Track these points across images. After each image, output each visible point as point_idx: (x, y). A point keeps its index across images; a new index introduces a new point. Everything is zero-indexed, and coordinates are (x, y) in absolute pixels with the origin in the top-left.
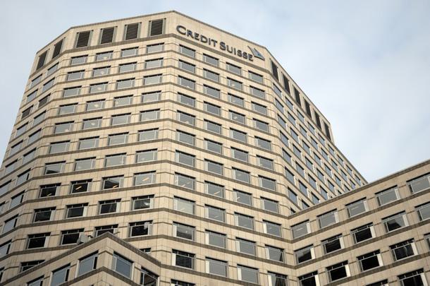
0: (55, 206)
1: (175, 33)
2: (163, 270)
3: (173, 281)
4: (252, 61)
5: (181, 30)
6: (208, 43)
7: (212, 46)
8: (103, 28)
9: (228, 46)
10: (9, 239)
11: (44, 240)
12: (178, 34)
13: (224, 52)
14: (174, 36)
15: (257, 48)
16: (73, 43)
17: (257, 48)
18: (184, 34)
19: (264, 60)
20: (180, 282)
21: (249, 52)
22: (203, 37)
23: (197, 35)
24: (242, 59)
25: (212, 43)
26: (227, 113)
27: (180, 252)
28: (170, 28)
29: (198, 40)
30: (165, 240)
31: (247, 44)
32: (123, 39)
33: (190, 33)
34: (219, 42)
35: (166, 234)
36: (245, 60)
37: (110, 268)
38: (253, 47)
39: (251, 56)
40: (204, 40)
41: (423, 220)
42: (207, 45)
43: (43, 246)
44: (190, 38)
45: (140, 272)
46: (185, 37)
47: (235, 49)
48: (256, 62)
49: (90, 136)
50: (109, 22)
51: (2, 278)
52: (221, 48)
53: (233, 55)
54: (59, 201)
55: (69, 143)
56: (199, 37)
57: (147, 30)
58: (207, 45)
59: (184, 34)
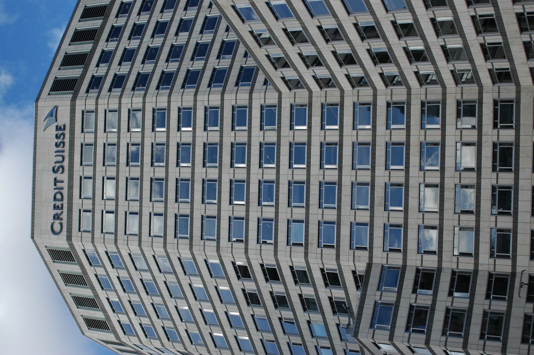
4: (64, 126)
5: (57, 228)
6: (62, 191)
7: (65, 185)
15: (365, 349)
17: (365, 349)
18: (61, 224)
19: (56, 107)
22: (55, 199)
24: (67, 140)
27: (451, 286)
29: (62, 205)
31: (40, 132)
32: (88, 288)
33: (57, 217)
37: (172, 13)
39: (58, 128)
40: (59, 196)
42: (65, 192)
48: (64, 119)
51: (396, 342)
53: (66, 154)
55: (167, 282)
56: (59, 203)
58: (65, 192)
59: (61, 224)
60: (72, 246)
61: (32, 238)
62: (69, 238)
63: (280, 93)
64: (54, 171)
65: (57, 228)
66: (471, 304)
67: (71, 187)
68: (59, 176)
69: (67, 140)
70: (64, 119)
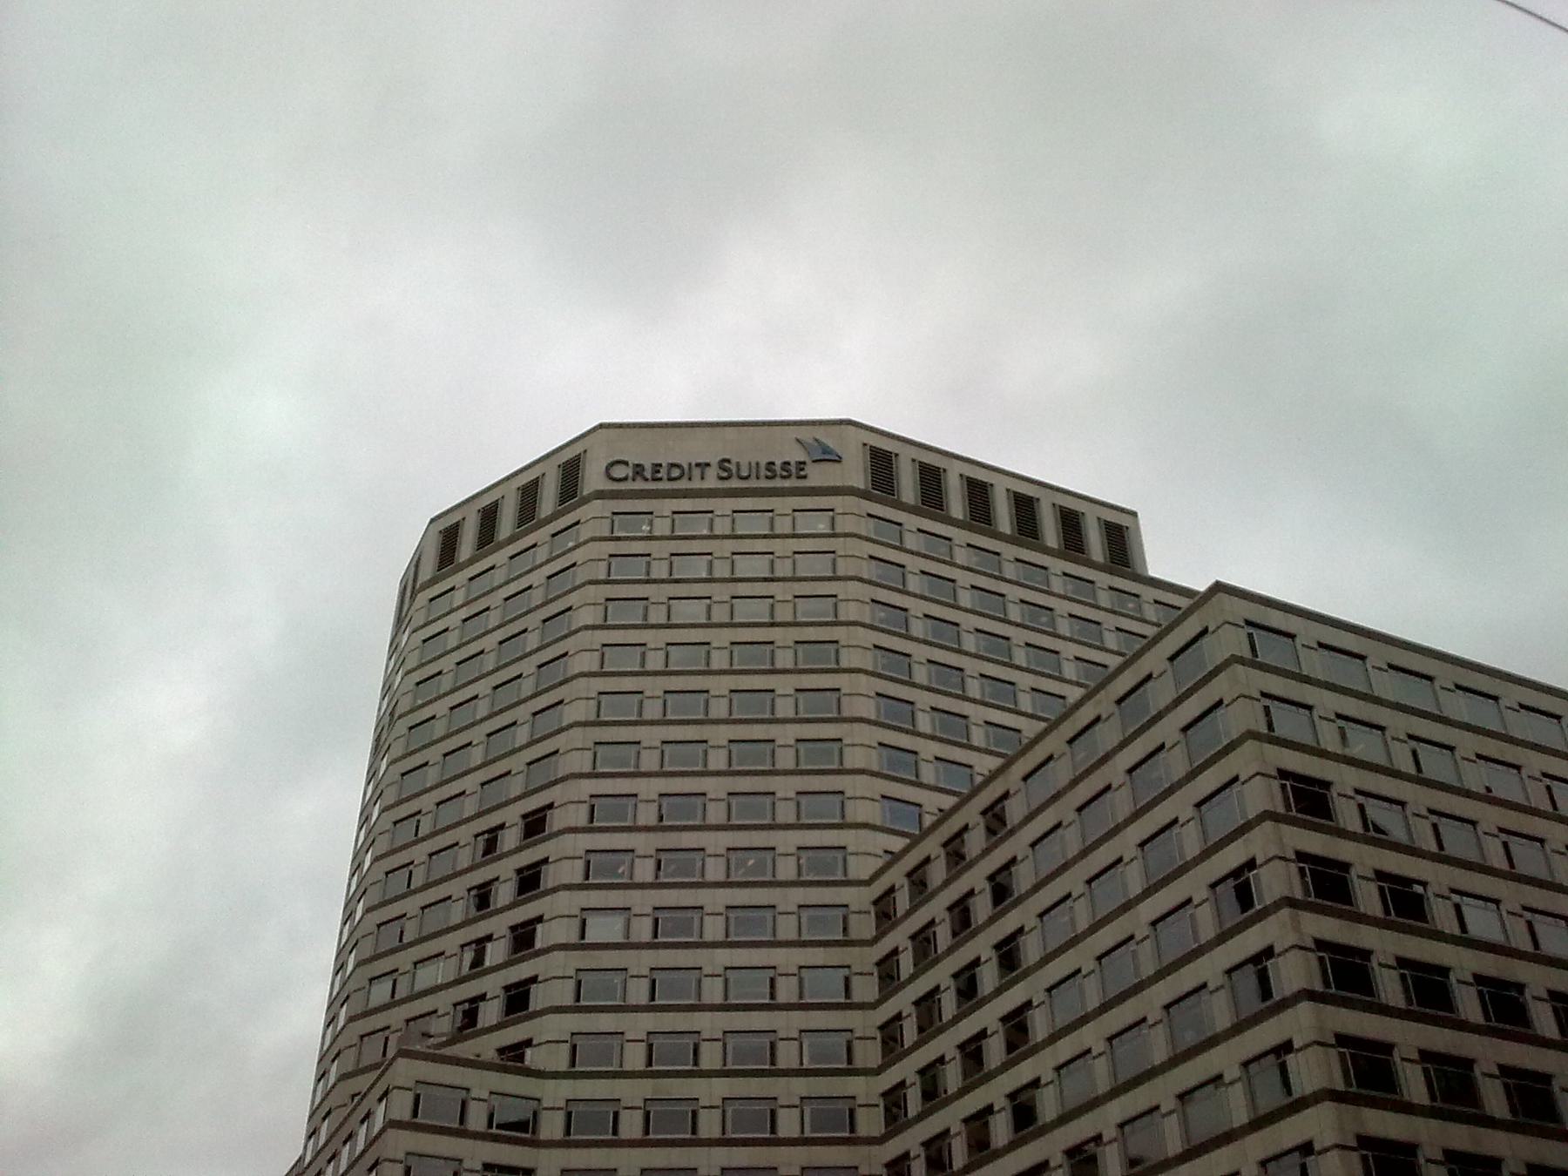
0: (489, 932)
1: (601, 487)
3: (488, 1167)
4: (805, 477)
5: (619, 472)
7: (697, 484)
9: (738, 464)
11: (527, 993)
14: (601, 495)
18: (625, 479)
19: (839, 460)
20: (502, 1168)
21: (796, 455)
23: (657, 467)
24: (778, 483)
25: (696, 472)
26: (1012, 566)
28: (593, 480)
31: (793, 433)
33: (639, 470)
36: (787, 484)
38: (806, 434)
40: (676, 473)
41: (651, 1136)
43: (527, 1008)
44: (639, 485)
45: (1333, 1052)
47: (757, 464)
48: (818, 476)
52: (722, 478)
53: (753, 483)
56: (663, 473)
58: (683, 484)
59: (625, 479)
60: (585, 501)
61: (601, 426)
62: (601, 495)
63: (867, 883)
65: (619, 472)
68: (712, 473)
69: (778, 483)
70: (818, 476)
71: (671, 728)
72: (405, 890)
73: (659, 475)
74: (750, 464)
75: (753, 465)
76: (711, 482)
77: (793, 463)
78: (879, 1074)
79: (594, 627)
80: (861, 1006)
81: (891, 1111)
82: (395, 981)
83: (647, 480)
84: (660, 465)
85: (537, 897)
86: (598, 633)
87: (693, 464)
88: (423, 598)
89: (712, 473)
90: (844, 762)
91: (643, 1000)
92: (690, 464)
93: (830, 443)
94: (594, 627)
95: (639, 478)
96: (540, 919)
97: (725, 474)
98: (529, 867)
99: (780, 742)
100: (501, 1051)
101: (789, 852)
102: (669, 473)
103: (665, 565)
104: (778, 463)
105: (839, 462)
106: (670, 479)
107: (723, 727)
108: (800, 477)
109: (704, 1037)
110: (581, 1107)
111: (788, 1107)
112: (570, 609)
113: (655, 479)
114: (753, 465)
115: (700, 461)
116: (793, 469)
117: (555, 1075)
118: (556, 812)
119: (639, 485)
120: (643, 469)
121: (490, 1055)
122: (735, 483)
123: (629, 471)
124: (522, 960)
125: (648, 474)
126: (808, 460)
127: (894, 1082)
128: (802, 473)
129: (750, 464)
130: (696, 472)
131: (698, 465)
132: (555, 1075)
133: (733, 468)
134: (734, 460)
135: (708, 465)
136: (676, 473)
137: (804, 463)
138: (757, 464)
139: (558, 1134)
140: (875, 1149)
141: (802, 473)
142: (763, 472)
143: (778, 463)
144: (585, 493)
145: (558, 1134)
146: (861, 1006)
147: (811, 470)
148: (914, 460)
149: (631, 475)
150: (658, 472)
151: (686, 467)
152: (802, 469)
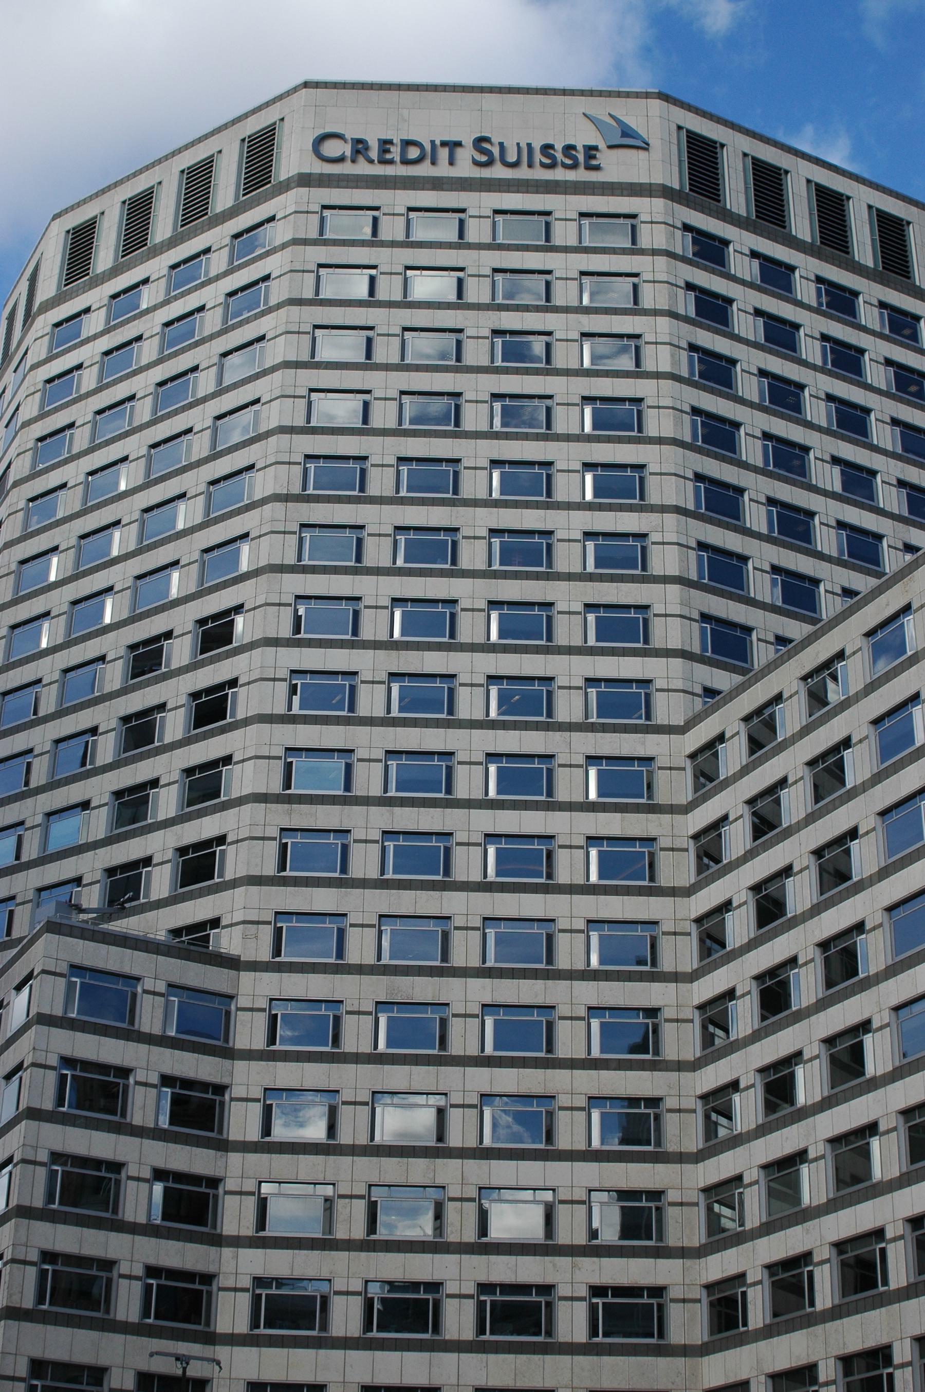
2: (246, 978)
4: (597, 168)
5: (332, 148)
6: (428, 161)
7: (443, 170)
8: (185, 166)
9: (501, 145)
10: (25, 973)
12: (320, 168)
13: (486, 173)
14: (305, 180)
16: (57, 271)
18: (341, 160)
21: (585, 136)
23: (385, 145)
24: (560, 174)
29: (391, 162)
30: (254, 889)
31: (581, 104)
33: (360, 148)
34: (468, 141)
35: (256, 872)
39: (591, 151)
42: (424, 170)
45: (696, 626)
46: (347, 168)
49: (25, 681)
50: (246, 116)
52: (476, 163)
53: (523, 173)
54: (237, 734)
56: (395, 152)
57: (233, 179)
58: (424, 170)
59: (341, 160)
60: (284, 187)
61: (306, 85)
62: (305, 180)
64: (480, 142)
65: (332, 148)
66: (133, 1229)
67: (437, 184)
68: (466, 155)
69: (560, 174)
71: (411, 440)
72: (10, 861)
73: (388, 156)
74: (518, 144)
75: (524, 146)
76: (464, 168)
77: (580, 148)
78: (684, 733)
79: (281, 569)
80: (673, 892)
81: (702, 860)
82: (20, 837)
83: (371, 161)
84: (390, 142)
85: (223, 730)
86: (298, 438)
87: (438, 143)
88: (43, 323)
89: (466, 155)
90: (643, 364)
91: (359, 1232)
92: (433, 142)
93: (632, 122)
94: (281, 569)
95: (361, 159)
96: (238, 609)
97: (484, 159)
98: (215, 617)
99: (561, 681)
100: (176, 932)
101: (576, 1197)
102: (403, 153)
103: (401, 222)
104: (559, 147)
105: (646, 149)
106: (406, 162)
107: (481, 512)
108: (589, 168)
109: (452, 1195)
110: (290, 1009)
111: (571, 1018)
112: (261, 338)
113: (383, 162)
114: (524, 146)
115: (446, 138)
116: (581, 158)
117: (255, 966)
118: (242, 692)
119: (362, 168)
120: (367, 148)
121: (161, 936)
122: (498, 172)
123: (347, 150)
124: (200, 814)
125: (374, 154)
126: (602, 145)
127: (725, 1174)
128: (594, 162)
129: (518, 144)
130: (444, 153)
131: (444, 144)
132: (255, 966)
133: (496, 151)
134: (495, 140)
135: (458, 144)
136: (413, 153)
137: (595, 148)
138: (529, 145)
139: (259, 1042)
140: (686, 1076)
141: (594, 162)
142: (538, 157)
143: (559, 147)
144: (283, 177)
145: (259, 1042)
146: (673, 892)
147: (605, 158)
148: (745, 155)
149: (348, 153)
150: (388, 151)
151: (428, 147)
152: (594, 157)
